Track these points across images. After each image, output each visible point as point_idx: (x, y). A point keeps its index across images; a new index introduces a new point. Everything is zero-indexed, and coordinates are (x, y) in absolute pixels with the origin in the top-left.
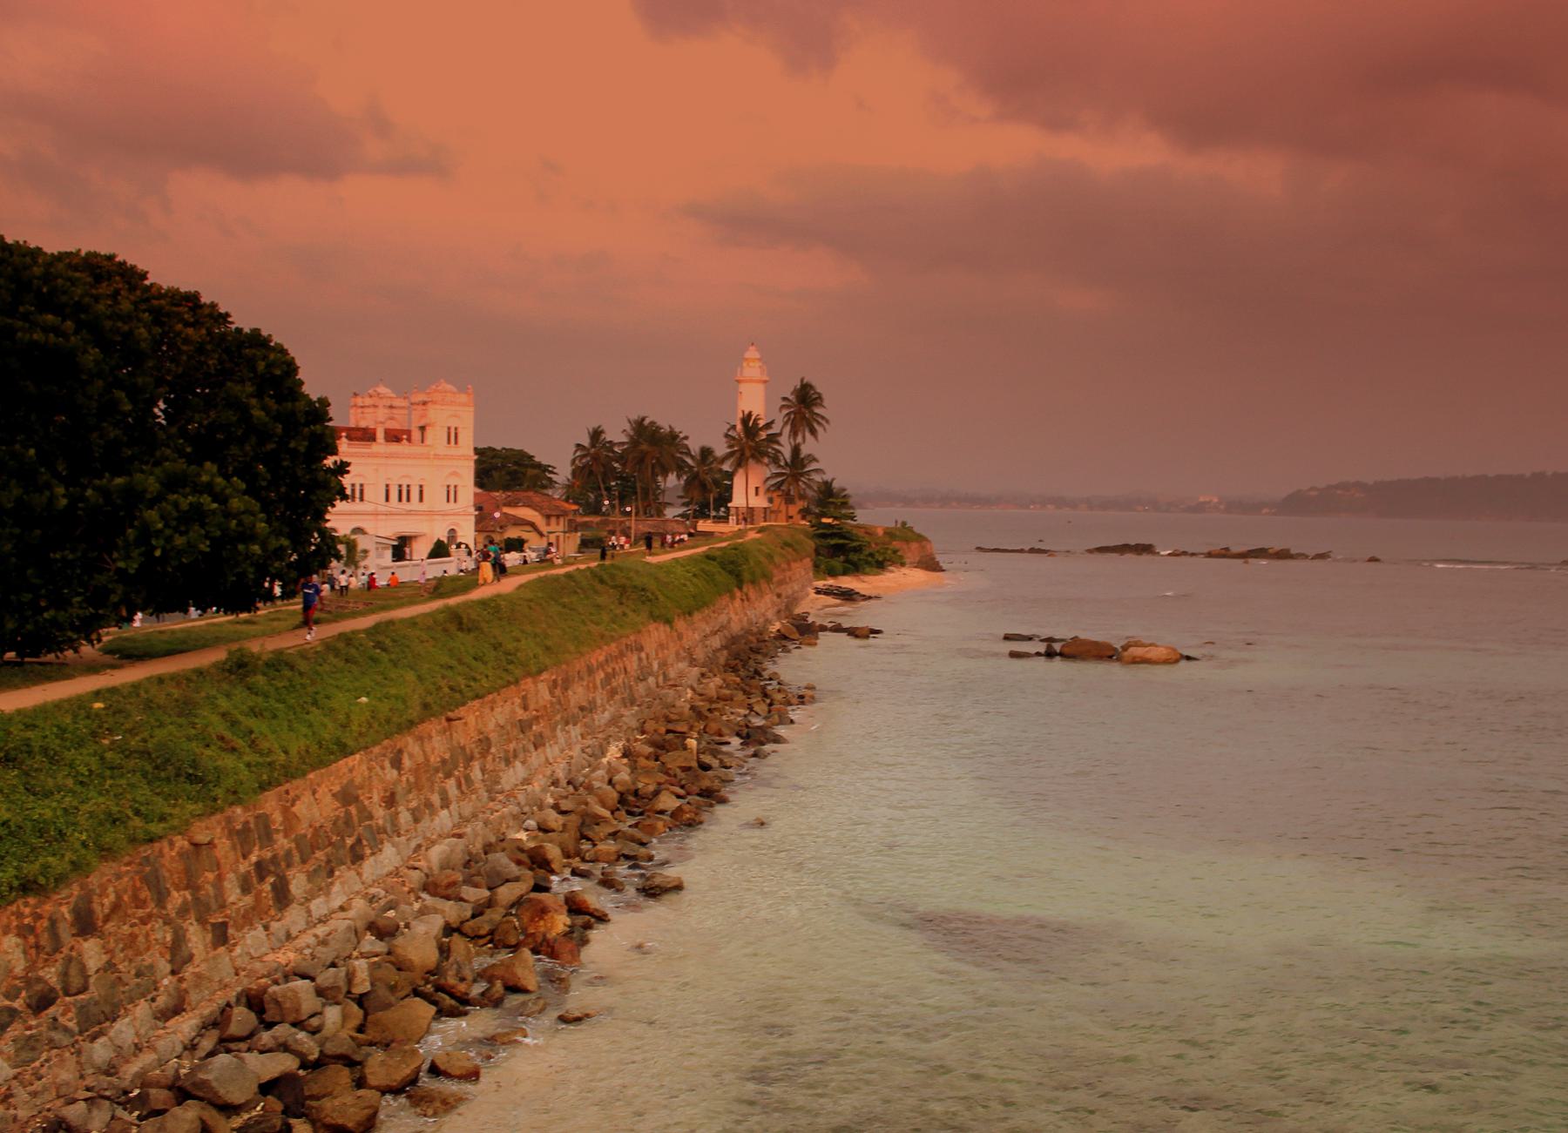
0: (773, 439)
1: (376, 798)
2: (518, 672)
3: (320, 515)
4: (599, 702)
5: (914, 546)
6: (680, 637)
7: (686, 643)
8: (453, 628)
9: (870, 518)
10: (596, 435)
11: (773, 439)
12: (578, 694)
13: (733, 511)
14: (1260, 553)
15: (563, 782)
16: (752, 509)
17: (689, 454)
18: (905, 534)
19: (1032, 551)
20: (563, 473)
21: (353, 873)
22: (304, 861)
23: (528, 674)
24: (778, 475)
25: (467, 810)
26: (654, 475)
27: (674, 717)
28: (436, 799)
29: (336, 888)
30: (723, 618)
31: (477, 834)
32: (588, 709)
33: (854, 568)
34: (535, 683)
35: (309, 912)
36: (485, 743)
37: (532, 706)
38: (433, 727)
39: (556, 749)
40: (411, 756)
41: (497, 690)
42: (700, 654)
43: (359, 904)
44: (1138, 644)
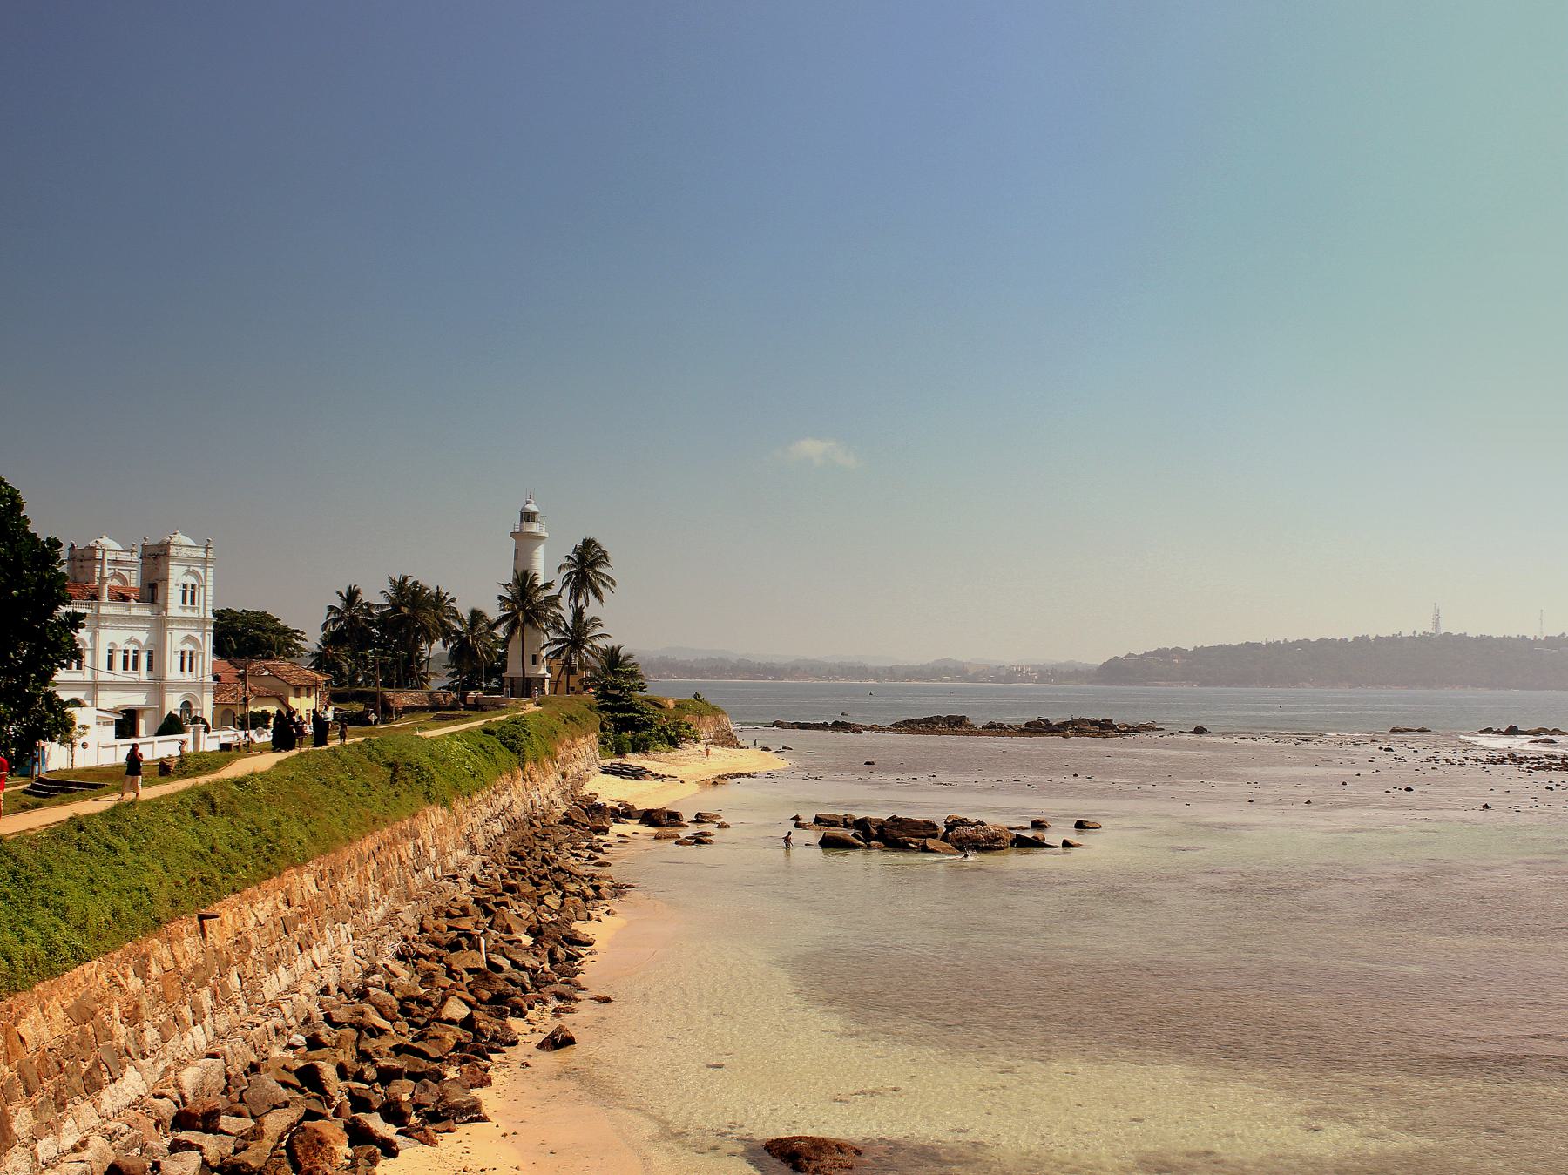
0: (553, 601)
1: (117, 1013)
2: (282, 863)
3: (46, 677)
4: (371, 896)
5: (709, 719)
6: (459, 822)
7: (467, 829)
8: (204, 811)
9: (660, 687)
10: (352, 596)
11: (553, 601)
12: (349, 886)
13: (507, 682)
14: (1061, 729)
15: (334, 990)
16: (529, 679)
17: (456, 616)
18: (701, 706)
19: (857, 730)
20: (312, 640)
21: (88, 1105)
22: (29, 1093)
23: (294, 864)
24: (557, 642)
25: (223, 1023)
26: (417, 642)
27: (457, 912)
28: (186, 1011)
29: (69, 1124)
30: (504, 800)
31: (240, 1053)
32: (359, 904)
33: (640, 747)
34: (300, 875)
35: (35, 1156)
36: (242, 942)
37: (297, 902)
38: (186, 927)
39: (324, 950)
40: (159, 961)
41: (257, 882)
42: (481, 842)
43: (97, 1142)
44: (963, 822)
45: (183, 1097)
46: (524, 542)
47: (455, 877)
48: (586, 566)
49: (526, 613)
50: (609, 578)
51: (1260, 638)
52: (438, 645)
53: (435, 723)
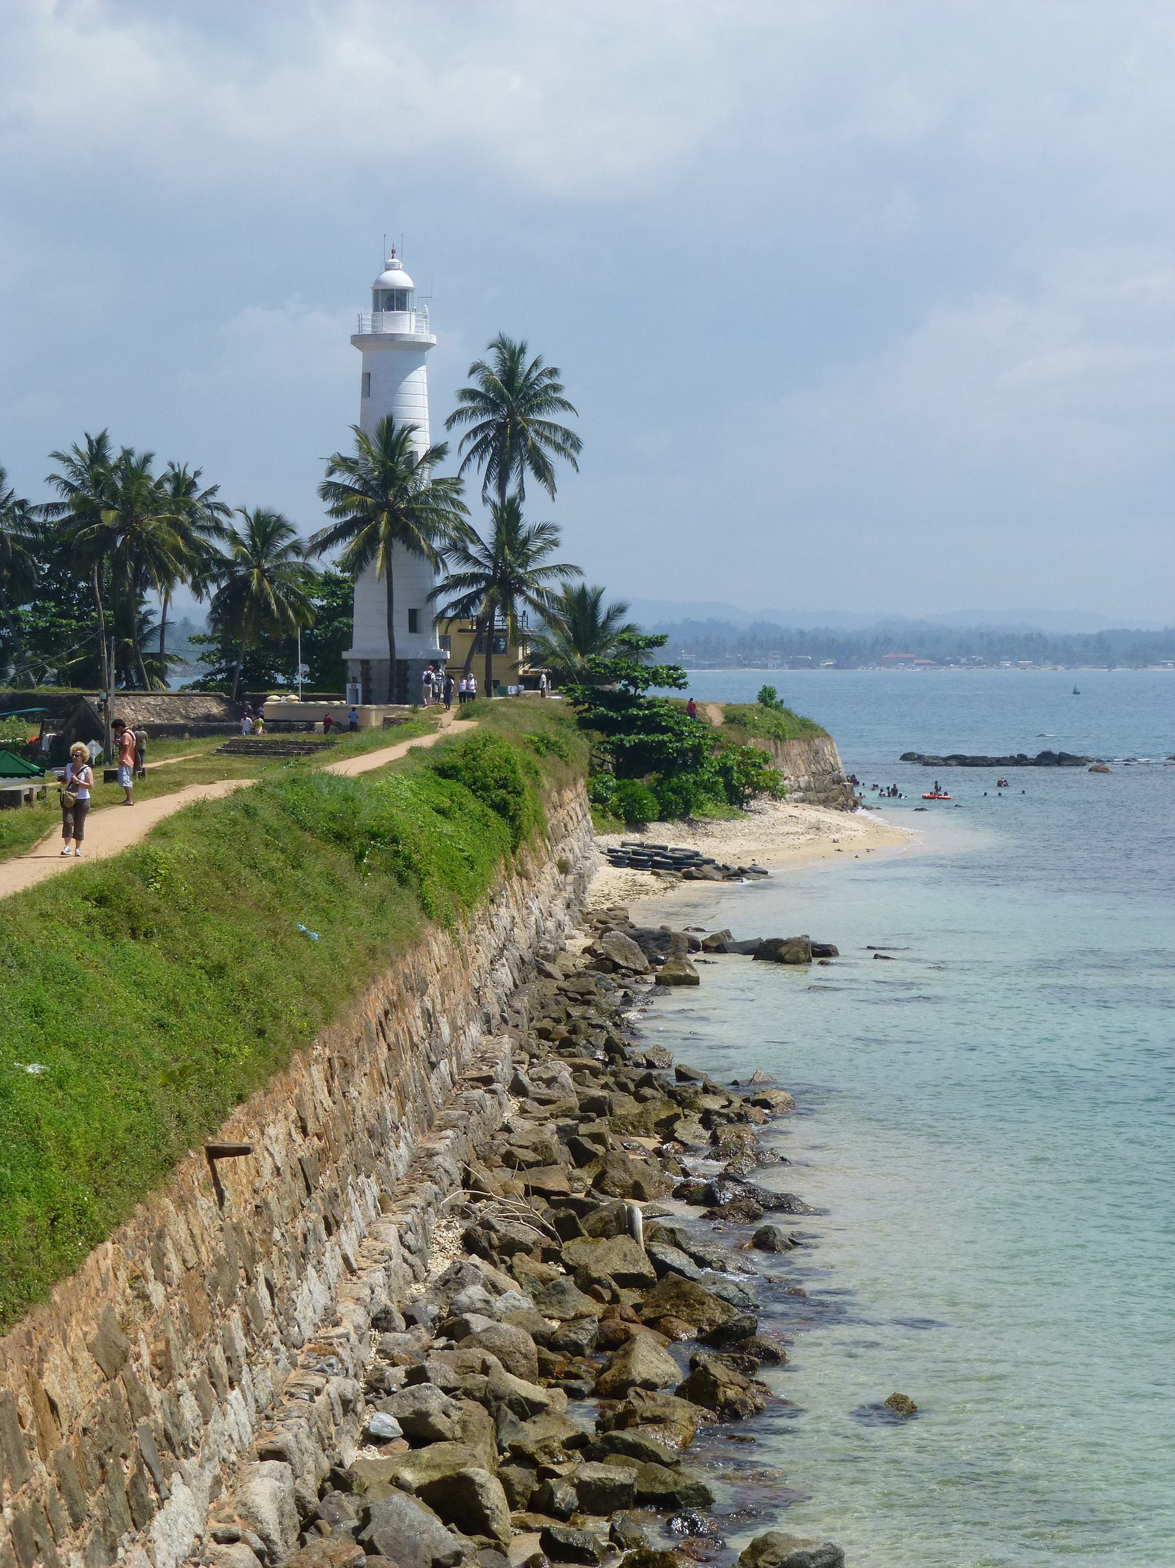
4: (389, 1116)
5: (796, 748)
9: (713, 690)
13: (354, 671)
33: (677, 809)
37: (311, 1126)
45: (265, 1539)
46: (386, 359)
47: (487, 1081)
48: (512, 410)
49: (394, 520)
50: (567, 435)
51: (354, 641)
52: (182, 592)
53: (225, 761)
